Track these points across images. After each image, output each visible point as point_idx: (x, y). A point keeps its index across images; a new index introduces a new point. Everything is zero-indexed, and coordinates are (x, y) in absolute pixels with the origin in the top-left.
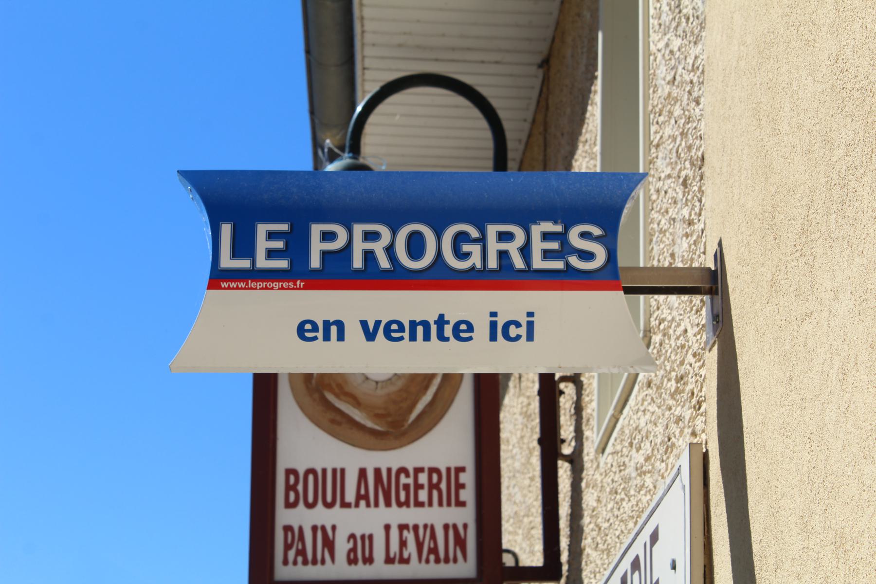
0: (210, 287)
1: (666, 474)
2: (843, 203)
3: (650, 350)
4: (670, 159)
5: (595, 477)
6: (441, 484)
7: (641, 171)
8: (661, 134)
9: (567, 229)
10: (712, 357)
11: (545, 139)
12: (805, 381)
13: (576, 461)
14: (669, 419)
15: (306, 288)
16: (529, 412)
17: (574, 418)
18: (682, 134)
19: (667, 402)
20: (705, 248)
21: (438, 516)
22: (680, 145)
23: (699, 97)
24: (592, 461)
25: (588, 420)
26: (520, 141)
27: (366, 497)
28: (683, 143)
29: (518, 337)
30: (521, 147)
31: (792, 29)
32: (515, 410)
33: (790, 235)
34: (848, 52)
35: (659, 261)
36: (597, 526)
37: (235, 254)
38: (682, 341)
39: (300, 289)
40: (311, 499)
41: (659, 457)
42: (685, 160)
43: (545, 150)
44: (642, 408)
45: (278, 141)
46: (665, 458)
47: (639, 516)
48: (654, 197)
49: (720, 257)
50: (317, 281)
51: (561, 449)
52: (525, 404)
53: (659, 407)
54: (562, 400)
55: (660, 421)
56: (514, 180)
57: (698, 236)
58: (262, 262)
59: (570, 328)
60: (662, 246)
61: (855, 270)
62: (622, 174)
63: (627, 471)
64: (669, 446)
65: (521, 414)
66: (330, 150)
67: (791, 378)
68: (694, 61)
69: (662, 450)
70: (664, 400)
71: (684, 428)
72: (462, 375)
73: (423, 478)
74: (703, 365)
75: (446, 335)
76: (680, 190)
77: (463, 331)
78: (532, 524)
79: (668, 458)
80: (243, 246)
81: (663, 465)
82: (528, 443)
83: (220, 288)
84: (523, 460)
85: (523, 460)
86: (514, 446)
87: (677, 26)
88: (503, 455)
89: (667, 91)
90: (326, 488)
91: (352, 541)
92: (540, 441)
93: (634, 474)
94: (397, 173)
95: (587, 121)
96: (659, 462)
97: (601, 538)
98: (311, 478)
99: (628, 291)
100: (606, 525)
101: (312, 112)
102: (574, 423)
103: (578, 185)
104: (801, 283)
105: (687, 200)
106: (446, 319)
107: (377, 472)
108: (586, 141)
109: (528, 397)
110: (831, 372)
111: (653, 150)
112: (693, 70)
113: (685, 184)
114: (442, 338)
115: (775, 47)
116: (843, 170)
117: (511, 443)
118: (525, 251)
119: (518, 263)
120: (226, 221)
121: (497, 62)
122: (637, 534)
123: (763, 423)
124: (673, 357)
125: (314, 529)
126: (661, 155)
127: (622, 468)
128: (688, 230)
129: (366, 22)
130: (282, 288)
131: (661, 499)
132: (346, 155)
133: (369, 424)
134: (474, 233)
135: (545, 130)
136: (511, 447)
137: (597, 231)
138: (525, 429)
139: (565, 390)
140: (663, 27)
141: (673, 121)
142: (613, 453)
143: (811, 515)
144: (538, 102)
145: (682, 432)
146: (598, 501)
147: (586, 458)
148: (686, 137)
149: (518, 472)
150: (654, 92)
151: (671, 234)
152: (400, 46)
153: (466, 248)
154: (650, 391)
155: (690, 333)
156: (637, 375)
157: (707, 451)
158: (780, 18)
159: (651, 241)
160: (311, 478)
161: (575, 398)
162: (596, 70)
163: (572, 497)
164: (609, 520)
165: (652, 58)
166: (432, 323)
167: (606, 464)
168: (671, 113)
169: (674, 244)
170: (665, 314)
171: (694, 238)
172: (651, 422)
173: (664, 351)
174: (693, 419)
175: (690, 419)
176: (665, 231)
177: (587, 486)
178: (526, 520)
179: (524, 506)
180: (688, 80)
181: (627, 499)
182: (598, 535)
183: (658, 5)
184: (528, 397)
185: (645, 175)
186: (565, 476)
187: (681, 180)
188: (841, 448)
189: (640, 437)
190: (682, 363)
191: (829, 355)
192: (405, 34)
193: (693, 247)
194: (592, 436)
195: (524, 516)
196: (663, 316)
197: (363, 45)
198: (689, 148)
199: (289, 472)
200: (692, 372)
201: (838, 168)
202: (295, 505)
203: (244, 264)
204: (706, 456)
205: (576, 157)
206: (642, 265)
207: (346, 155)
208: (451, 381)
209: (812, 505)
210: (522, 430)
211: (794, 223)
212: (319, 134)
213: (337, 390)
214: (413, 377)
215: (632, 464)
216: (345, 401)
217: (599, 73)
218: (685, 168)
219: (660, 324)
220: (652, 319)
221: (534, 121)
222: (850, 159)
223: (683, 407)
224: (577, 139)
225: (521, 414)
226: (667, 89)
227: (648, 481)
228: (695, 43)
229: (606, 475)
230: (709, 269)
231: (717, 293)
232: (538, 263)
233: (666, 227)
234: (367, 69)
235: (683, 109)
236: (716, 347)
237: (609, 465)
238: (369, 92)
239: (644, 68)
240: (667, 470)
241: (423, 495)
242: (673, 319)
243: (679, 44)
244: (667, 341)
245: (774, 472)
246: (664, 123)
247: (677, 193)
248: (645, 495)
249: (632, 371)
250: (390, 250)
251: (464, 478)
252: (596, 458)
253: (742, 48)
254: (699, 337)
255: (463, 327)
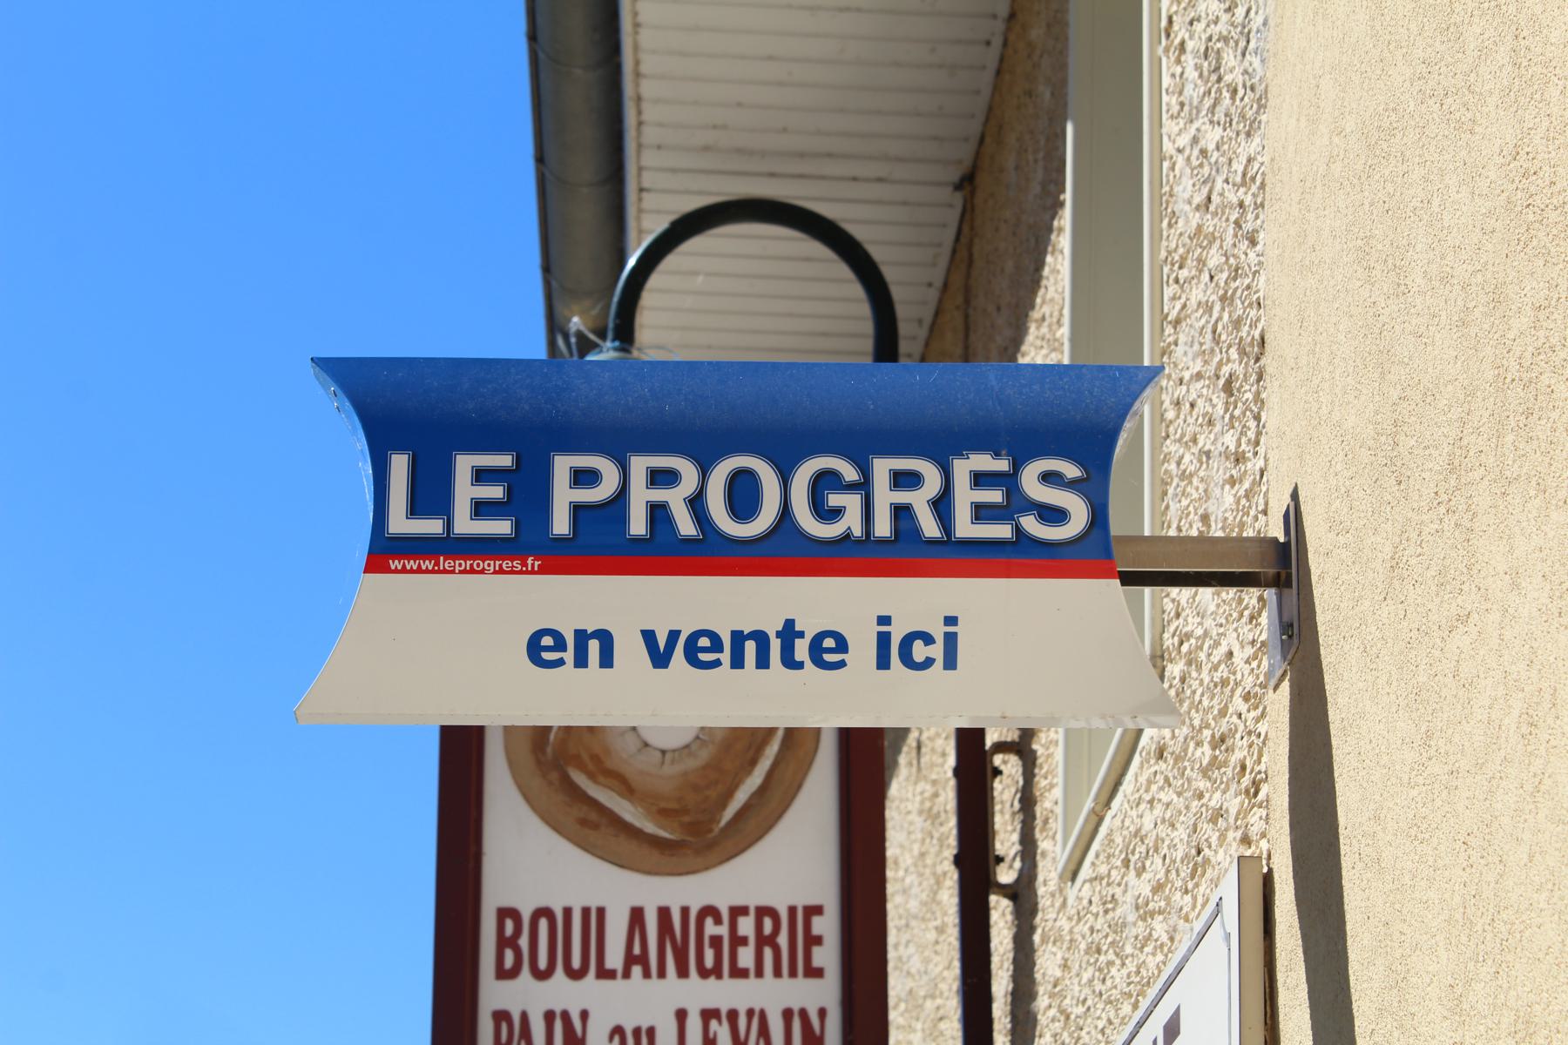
1: (1192, 915)
2: (1529, 413)
3: (1166, 685)
4: (1201, 344)
5: (1058, 924)
6: (779, 938)
10: (1280, 701)
11: (967, 316)
12: (1456, 739)
13: (1023, 896)
16: (935, 810)
17: (1019, 817)
20: (1266, 504)
21: (773, 994)
24: (1053, 895)
25: (1046, 821)
26: (920, 321)
27: (643, 960)
28: (1226, 316)
29: (929, 662)
30: (923, 333)
31: (1431, 102)
32: (910, 807)
33: (1426, 475)
34: (1537, 140)
36: (1062, 1012)
37: (416, 509)
38: (1223, 671)
39: (533, 572)
40: (543, 963)
41: (1179, 884)
42: (1230, 346)
43: (967, 336)
44: (1147, 797)
45: (487, 308)
46: (1190, 886)
47: (1141, 993)
48: (1170, 415)
49: (1294, 518)
52: (927, 795)
53: (1179, 794)
54: (997, 785)
55: (1182, 818)
56: (917, 382)
58: (465, 525)
59: (1022, 648)
60: (1185, 502)
61: (1551, 535)
62: (1118, 368)
63: (1119, 911)
64: (1198, 862)
65: (920, 812)
66: (580, 336)
67: (1429, 735)
68: (1246, 167)
69: (1185, 871)
70: (1189, 780)
72: (818, 730)
73: (746, 926)
74: (1263, 715)
75: (798, 658)
76: (1219, 400)
77: (828, 650)
78: (941, 1012)
79: (1197, 885)
80: (430, 494)
81: (1188, 898)
82: (934, 865)
83: (388, 570)
84: (924, 896)
85: (924, 896)
86: (906, 870)
87: (1214, 106)
88: (890, 888)
89: (1194, 224)
90: (570, 942)
91: (617, 1039)
92: (958, 861)
93: (1131, 918)
95: (1044, 282)
96: (1179, 894)
97: (1071, 1035)
98: (543, 924)
99: (1129, 579)
100: (1080, 1010)
101: (547, 269)
102: (1019, 827)
103: (1036, 387)
104: (1447, 562)
105: (1232, 417)
106: (797, 628)
107: (664, 913)
108: (1043, 319)
109: (934, 782)
110: (1506, 721)
111: (1169, 330)
112: (1244, 184)
113: (1228, 388)
114: (790, 662)
115: (1399, 136)
116: (1528, 355)
117: (902, 866)
118: (942, 505)
119: (930, 527)
120: (400, 449)
121: (880, 180)
122: (1140, 1025)
123: (1377, 818)
124: (1206, 703)
125: (549, 1016)
126: (1182, 338)
128: (1234, 472)
129: (645, 106)
130: (501, 571)
131: (1186, 959)
132: (609, 344)
133: (650, 827)
134: (850, 473)
135: (967, 301)
136: (901, 873)
137: (1071, 471)
139: (1002, 768)
140: (1186, 108)
141: (1205, 277)
143: (1468, 983)
144: (954, 252)
145: (1222, 837)
146: (1065, 966)
147: (1041, 891)
148: (1231, 304)
149: (915, 917)
150: (1170, 225)
151: (1202, 480)
152: (706, 149)
153: (834, 500)
154: (1162, 766)
155: (1238, 658)
156: (1140, 732)
157: (1270, 870)
158: (1407, 84)
159: (1165, 493)
160: (543, 924)
161: (1021, 783)
162: (1063, 191)
163: (1015, 961)
164: (1085, 1000)
165: (1166, 164)
166: (772, 636)
167: (1080, 899)
168: (1201, 262)
170: (1191, 624)
171: (1246, 485)
172: (1163, 821)
174: (1243, 813)
175: (1238, 813)
176: (1191, 475)
177: (1044, 940)
178: (929, 1004)
179: (925, 978)
180: (1235, 201)
181: (1118, 962)
182: (1064, 1029)
183: (1179, 70)
184: (934, 782)
185: (1156, 371)
186: (1002, 924)
187: (1222, 382)
188: (1525, 860)
189: (1143, 849)
190: (1223, 713)
191: (1501, 691)
192: (715, 127)
193: (1243, 501)
194: (1053, 851)
195: (925, 998)
196: (1188, 628)
197: (640, 146)
198: (1237, 324)
199: (505, 913)
200: (1241, 728)
201: (1517, 351)
202: (514, 973)
203: (432, 526)
204: (1268, 881)
205: (1024, 348)
206: (1147, 533)
207: (609, 344)
208: (798, 742)
209: (1471, 965)
210: (923, 841)
211: (1435, 453)
212: (560, 309)
213: (591, 766)
214: (736, 734)
215: (1129, 898)
216: (605, 786)
217: (1068, 197)
218: (1228, 360)
219: (1181, 643)
220: (1166, 635)
221: (946, 286)
222: (1541, 333)
223: (1224, 792)
224: (1027, 316)
225: (920, 812)
226: (1195, 219)
227: (1159, 928)
228: (1248, 134)
229: (1079, 920)
230: (1275, 540)
231: (1288, 584)
232: (965, 528)
234: (648, 190)
236: (1286, 685)
237: (1085, 902)
238: (650, 232)
239: (1151, 183)
241: (746, 957)
243: (1217, 138)
244: (1194, 674)
245: (1397, 906)
246: (1188, 280)
247: (1214, 406)
248: (1154, 954)
249: (1131, 726)
250: (696, 503)
251: (820, 925)
252: (1061, 891)
253: (1336, 140)
255: (829, 643)
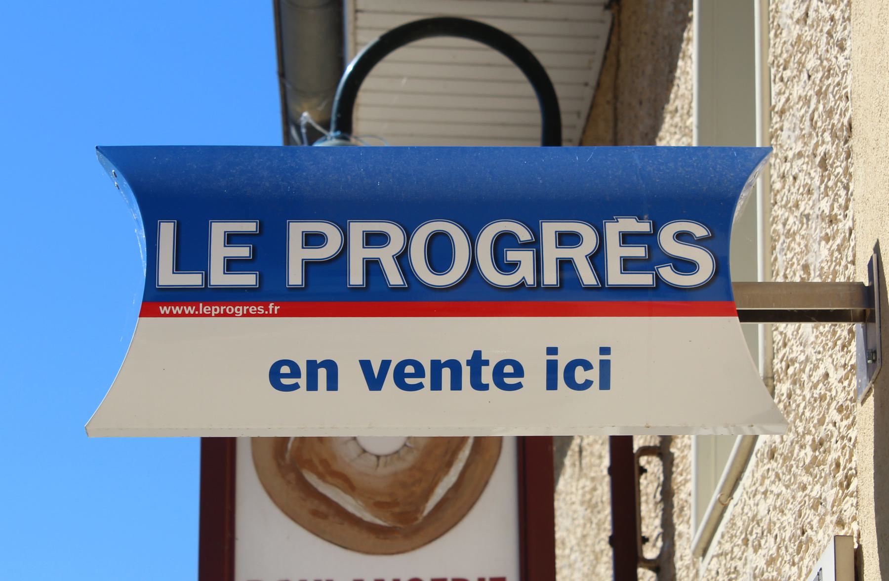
0: (144, 313)
3: (776, 400)
4: (802, 130)
7: (758, 145)
8: (786, 95)
9: (656, 228)
11: (615, 109)
14: (803, 503)
15: (281, 314)
16: (594, 501)
17: (661, 506)
18: (818, 93)
19: (799, 479)
20: (854, 256)
22: (816, 109)
23: (844, 39)
24: (688, 568)
25: (682, 509)
26: (579, 114)
28: (821, 107)
29: (588, 384)
30: (581, 123)
35: (785, 276)
38: (821, 389)
39: (273, 315)
41: (787, 558)
42: (824, 131)
44: (762, 489)
46: (796, 559)
48: (777, 186)
49: (876, 267)
50: (297, 304)
51: (642, 551)
52: (587, 489)
53: (787, 487)
54: (643, 480)
55: (790, 506)
57: (844, 239)
58: (219, 278)
59: (660, 372)
60: (789, 255)
62: (736, 149)
64: (803, 540)
66: (309, 127)
69: (792, 548)
70: (795, 476)
71: (825, 515)
72: (500, 439)
74: (853, 423)
77: (509, 374)
79: (802, 559)
80: (192, 255)
81: (795, 569)
82: (594, 545)
83: (158, 314)
84: (585, 569)
86: (572, 549)
88: (559, 563)
89: (795, 34)
92: (613, 541)
94: (412, 148)
95: (676, 82)
96: (787, 566)
99: (746, 316)
102: (660, 514)
103: (671, 165)
105: (826, 187)
108: (676, 110)
109: (593, 479)
111: (776, 118)
114: (478, 385)
117: (568, 545)
118: (597, 259)
119: (588, 277)
120: (167, 218)
124: (807, 414)
126: (786, 125)
127: (733, 576)
128: (828, 231)
130: (248, 315)
132: (332, 134)
133: (368, 517)
134: (524, 235)
135: (616, 97)
136: (567, 551)
137: (699, 231)
138: (588, 525)
139: (647, 467)
141: (804, 76)
142: (718, 556)
144: (605, 58)
145: (822, 521)
147: (678, 564)
150: (776, 36)
153: (512, 255)
154: (774, 464)
155: (833, 378)
156: (755, 438)
157: (860, 547)
159: (774, 248)
161: (662, 479)
162: (691, 9)
167: (709, 570)
168: (801, 64)
169: (808, 252)
170: (796, 351)
171: (838, 241)
172: (775, 508)
173: (794, 406)
174: (838, 501)
175: (834, 501)
176: (794, 234)
180: (827, 15)
184: (593, 479)
185: (766, 152)
187: (818, 159)
189: (759, 530)
190: (821, 422)
193: (836, 254)
194: (688, 533)
196: (793, 355)
198: (830, 113)
200: (836, 433)
204: (858, 555)
205: (661, 134)
206: (760, 280)
207: (332, 134)
208: (484, 448)
210: (584, 525)
212: (293, 107)
213: (321, 468)
215: (748, 569)
216: (332, 484)
217: (695, 13)
218: (823, 142)
219: (788, 367)
220: (775, 361)
221: (599, 85)
224: (663, 108)
226: (796, 30)
230: (862, 284)
231: (872, 320)
232: (615, 277)
233: (795, 228)
235: (820, 58)
236: (871, 400)
237: (713, 573)
238: (364, 44)
240: (800, 576)
242: (807, 359)
244: (798, 392)
247: (812, 179)
249: (749, 433)
250: (403, 259)
252: (694, 564)
254: (846, 383)
